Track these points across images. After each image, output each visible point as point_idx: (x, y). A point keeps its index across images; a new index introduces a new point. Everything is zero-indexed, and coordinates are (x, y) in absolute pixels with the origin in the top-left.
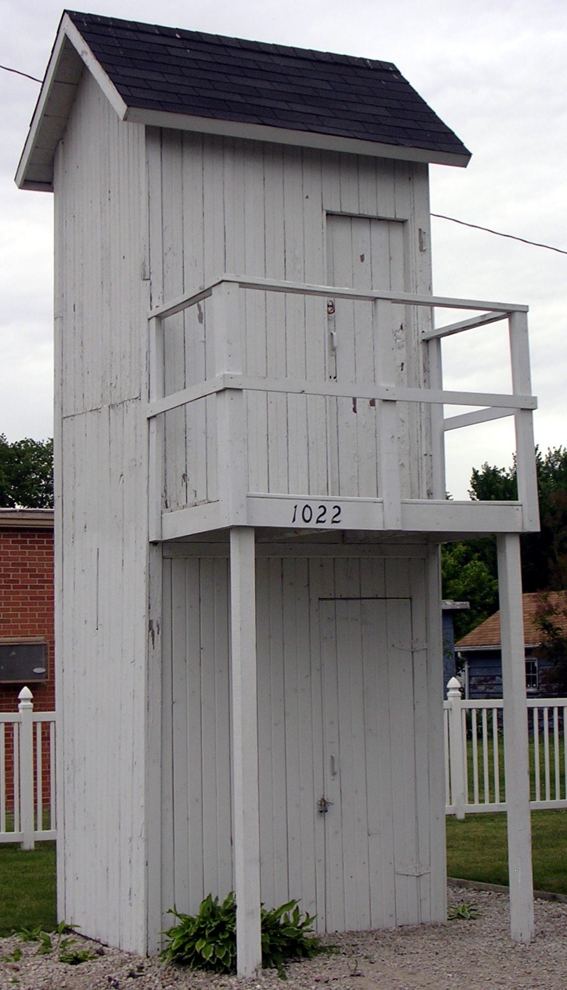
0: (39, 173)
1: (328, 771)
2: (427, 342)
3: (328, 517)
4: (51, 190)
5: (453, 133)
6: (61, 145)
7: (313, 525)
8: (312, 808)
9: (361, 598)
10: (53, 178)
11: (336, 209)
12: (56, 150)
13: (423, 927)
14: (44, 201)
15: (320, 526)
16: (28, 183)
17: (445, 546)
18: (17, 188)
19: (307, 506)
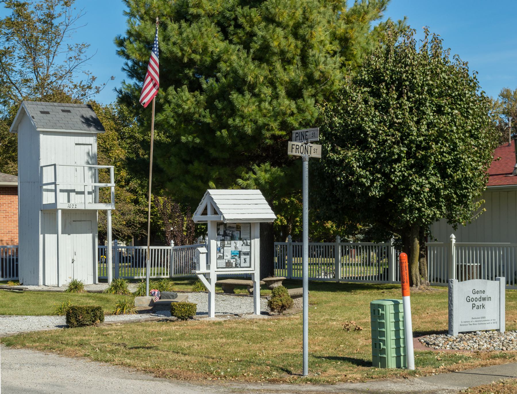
3: (74, 206)
6: (19, 126)
7: (71, 208)
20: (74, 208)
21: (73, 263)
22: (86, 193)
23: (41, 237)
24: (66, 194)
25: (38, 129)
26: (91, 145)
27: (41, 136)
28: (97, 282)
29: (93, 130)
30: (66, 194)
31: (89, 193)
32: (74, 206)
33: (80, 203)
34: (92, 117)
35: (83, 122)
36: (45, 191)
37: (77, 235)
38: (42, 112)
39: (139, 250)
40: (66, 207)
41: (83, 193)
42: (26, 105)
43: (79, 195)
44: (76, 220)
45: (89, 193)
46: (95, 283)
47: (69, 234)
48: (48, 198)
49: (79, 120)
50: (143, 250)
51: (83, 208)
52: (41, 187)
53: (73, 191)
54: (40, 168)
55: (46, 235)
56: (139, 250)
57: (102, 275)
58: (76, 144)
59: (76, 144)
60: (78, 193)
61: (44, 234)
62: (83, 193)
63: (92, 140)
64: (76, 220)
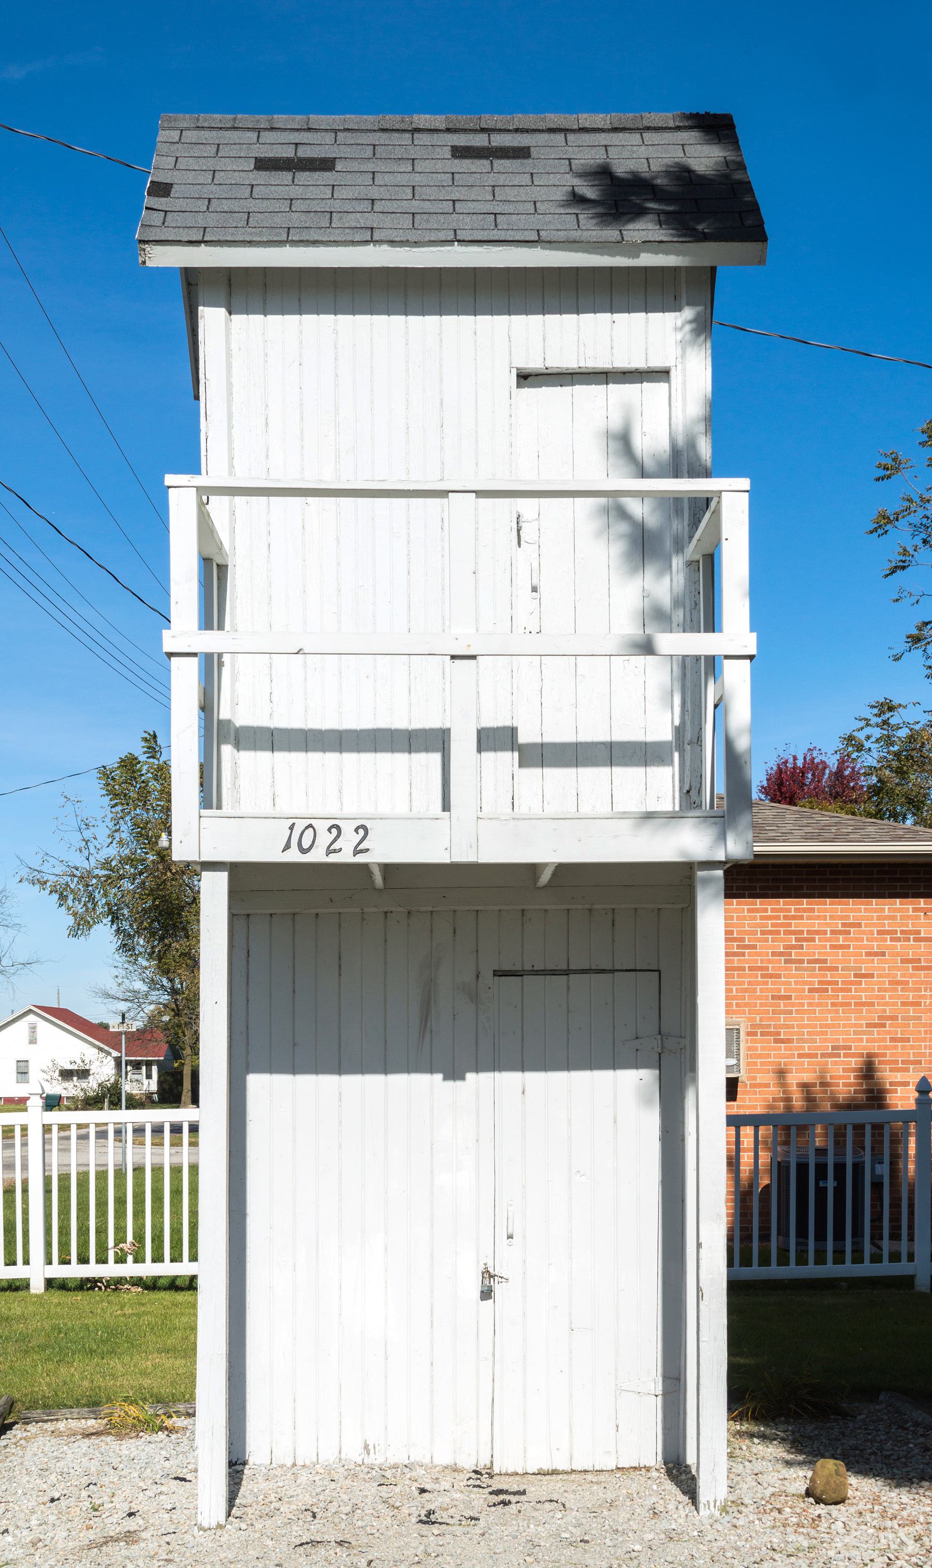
7: (317, 856)
9: (567, 972)
11: (534, 363)
15: (333, 858)
19: (310, 826)
20: (346, 856)
21: (487, 1294)
26: (662, 374)
29: (648, 245)
37: (534, 1078)
47: (454, 1074)
58: (525, 378)
59: (525, 378)
63: (658, 336)
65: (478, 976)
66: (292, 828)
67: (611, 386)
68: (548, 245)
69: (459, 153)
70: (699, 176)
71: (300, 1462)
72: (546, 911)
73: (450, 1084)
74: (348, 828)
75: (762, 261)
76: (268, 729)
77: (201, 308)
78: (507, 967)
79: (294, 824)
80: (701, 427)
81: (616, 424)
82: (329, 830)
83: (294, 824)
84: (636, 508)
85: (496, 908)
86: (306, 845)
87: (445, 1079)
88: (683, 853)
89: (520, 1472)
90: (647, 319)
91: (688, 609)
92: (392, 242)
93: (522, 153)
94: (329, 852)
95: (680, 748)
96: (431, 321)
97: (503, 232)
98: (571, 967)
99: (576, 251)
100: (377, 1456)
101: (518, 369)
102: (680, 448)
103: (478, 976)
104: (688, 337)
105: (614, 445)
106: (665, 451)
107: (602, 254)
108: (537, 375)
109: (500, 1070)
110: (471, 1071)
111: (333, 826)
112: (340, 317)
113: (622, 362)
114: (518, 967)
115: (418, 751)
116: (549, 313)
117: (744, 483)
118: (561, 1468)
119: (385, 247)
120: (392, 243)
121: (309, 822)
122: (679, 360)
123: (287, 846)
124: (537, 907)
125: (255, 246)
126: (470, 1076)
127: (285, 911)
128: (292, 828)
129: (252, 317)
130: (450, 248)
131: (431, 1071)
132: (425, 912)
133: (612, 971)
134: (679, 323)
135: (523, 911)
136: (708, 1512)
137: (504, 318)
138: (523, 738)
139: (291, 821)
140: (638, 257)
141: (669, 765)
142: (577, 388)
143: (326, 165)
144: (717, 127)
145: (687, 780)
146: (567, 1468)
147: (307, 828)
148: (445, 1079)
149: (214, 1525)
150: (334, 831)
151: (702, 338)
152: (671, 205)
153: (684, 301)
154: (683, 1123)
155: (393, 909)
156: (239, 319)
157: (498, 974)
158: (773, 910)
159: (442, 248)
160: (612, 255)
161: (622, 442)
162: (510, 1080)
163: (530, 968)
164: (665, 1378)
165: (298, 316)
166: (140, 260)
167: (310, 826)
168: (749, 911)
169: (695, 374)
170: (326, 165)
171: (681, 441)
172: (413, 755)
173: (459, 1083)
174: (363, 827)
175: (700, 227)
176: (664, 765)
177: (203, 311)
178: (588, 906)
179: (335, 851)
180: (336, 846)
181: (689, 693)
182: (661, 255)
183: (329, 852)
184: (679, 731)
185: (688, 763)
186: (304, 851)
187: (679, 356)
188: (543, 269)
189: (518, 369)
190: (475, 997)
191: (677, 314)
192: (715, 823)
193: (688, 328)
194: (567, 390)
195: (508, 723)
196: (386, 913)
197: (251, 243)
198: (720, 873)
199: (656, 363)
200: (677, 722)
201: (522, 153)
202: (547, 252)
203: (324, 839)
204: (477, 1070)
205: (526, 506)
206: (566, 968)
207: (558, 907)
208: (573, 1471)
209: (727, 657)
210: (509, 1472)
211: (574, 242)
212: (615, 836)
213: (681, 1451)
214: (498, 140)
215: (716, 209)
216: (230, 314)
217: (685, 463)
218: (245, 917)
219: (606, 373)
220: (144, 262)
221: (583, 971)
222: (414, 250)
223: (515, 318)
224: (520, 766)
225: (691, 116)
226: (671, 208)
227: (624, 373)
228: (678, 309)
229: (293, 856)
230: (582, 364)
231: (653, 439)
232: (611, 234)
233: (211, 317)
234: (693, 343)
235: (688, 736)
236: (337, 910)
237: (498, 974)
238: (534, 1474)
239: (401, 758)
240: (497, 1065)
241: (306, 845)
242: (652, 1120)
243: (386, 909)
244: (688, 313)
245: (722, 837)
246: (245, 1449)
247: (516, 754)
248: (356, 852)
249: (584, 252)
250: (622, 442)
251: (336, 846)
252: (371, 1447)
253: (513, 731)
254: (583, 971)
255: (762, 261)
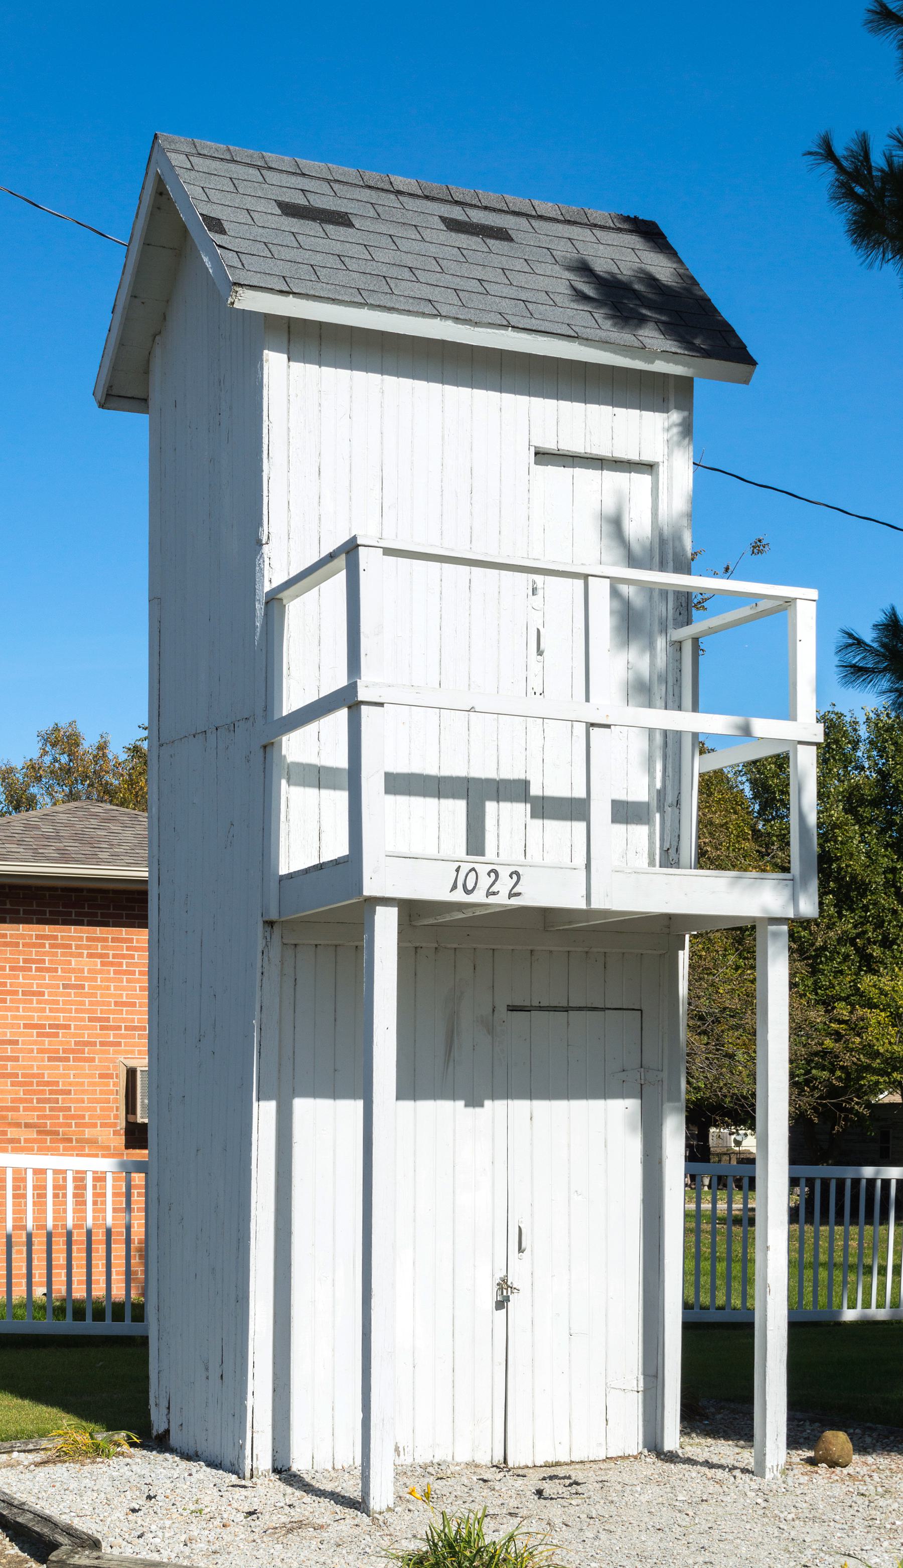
0: (122, 391)
1: (514, 1246)
2: (265, 747)
3: (504, 885)
4: (145, 410)
5: (732, 331)
6: (158, 351)
7: (479, 897)
8: (489, 1297)
9: (566, 1009)
10: (148, 392)
11: (550, 445)
12: (148, 361)
13: (628, 1457)
14: (135, 426)
15: (492, 900)
16: (113, 396)
17: (695, 937)
18: (96, 405)
19: (473, 869)
20: (502, 899)
21: (501, 1304)
22: (600, 811)
23: (264, 1114)
24: (459, 807)
25: (249, 301)
26: (649, 467)
27: (283, 377)
28: (672, 1439)
29: (656, 352)
30: (459, 807)
31: (625, 813)
32: (504, 885)
33: (547, 869)
34: (651, 280)
35: (581, 297)
36: (304, 783)
37: (541, 1106)
38: (289, 210)
39: (841, 1183)
40: (434, 887)
41: (574, 809)
42: (177, 160)
43: (552, 825)
44: (522, 995)
45: (625, 813)
46: (654, 1445)
47: (474, 1102)
48: (307, 829)
49: (561, 282)
50: (856, 1182)
51: (570, 898)
52: (269, 748)
53: (514, 790)
54: (261, 598)
55: (302, 1106)
56: (841, 1183)
57: (705, 1299)
58: (543, 456)
59: (543, 456)
60: (547, 808)
61: (258, 1100)
62: (574, 809)
63: (645, 431)
64: (522, 995)
65: (494, 1011)
66: (458, 870)
67: (605, 472)
68: (585, 342)
69: (453, 225)
70: (664, 285)
71: (338, 1466)
72: (551, 952)
73: (470, 1110)
74: (504, 873)
75: (746, 381)
76: (315, 766)
77: (266, 352)
78: (518, 1002)
79: (459, 867)
80: (685, 522)
81: (610, 507)
82: (489, 874)
83: (459, 867)
84: (624, 589)
85: (511, 947)
86: (470, 886)
87: (466, 1106)
88: (764, 910)
89: (530, 1465)
90: (641, 416)
91: (670, 683)
92: (457, 319)
93: (502, 235)
94: (489, 894)
95: (661, 809)
96: (464, 392)
97: (538, 322)
98: (571, 1005)
99: (605, 351)
100: (406, 1457)
101: (535, 447)
102: (665, 538)
103: (494, 1011)
104: (675, 438)
105: (606, 528)
106: (647, 538)
107: (625, 356)
108: (544, 454)
109: (512, 1098)
110: (488, 1099)
111: (492, 871)
112: (386, 377)
113: (621, 453)
114: (527, 1003)
115: (447, 797)
116: (562, 399)
117: (813, 594)
118: (562, 1460)
119: (450, 323)
120: (456, 320)
121: (472, 865)
122: (666, 457)
123: (454, 887)
124: (544, 948)
125: (337, 304)
126: (487, 1103)
127: (329, 942)
128: (458, 870)
129: (309, 366)
130: (503, 332)
131: (454, 1098)
132: (451, 949)
133: (604, 1009)
134: (666, 425)
135: (532, 951)
136: (772, 1475)
137: (525, 399)
138: (535, 791)
139: (458, 864)
140: (653, 363)
141: (645, 824)
142: (577, 470)
143: (342, 219)
144: (650, 233)
145: (667, 838)
146: (567, 1460)
147: (470, 871)
148: (466, 1106)
149: (384, 1508)
150: (493, 875)
151: (687, 440)
152: (660, 313)
153: (672, 403)
154: (661, 1148)
155: (424, 945)
156: (297, 366)
157: (512, 1009)
158: (89, 939)
159: (497, 331)
160: (633, 358)
161: (615, 525)
162: (521, 1107)
163: (537, 1004)
164: (645, 1374)
165: (349, 371)
166: (230, 300)
167: (473, 869)
168: (38, 937)
169: (679, 474)
170: (342, 219)
171: (666, 531)
172: (442, 800)
173: (478, 1110)
174: (516, 873)
175: (697, 342)
176: (642, 824)
177: (267, 355)
178: (586, 949)
179: (494, 894)
180: (494, 889)
181: (670, 761)
182: (671, 364)
183: (489, 894)
184: (661, 794)
185: (668, 824)
186: (468, 892)
187: (666, 453)
188: (572, 360)
189: (535, 447)
190: (491, 1030)
191: (665, 415)
192: (787, 885)
193: (675, 430)
194: (569, 471)
195: (522, 777)
196: (416, 948)
197: (333, 301)
198: (785, 928)
199: (646, 457)
200: (658, 785)
201: (502, 235)
202: (582, 348)
203: (485, 882)
204: (493, 1098)
205: (539, 579)
206: (566, 1005)
207: (561, 949)
208: (572, 1462)
209: (800, 743)
210: (521, 1465)
211: (607, 342)
212: (714, 892)
213: (659, 1441)
214: (478, 217)
215: (697, 324)
216: (289, 360)
217: (671, 551)
218: (293, 947)
219: (601, 460)
220: (233, 303)
221: (580, 1009)
222: (476, 329)
223: (534, 400)
224: (532, 817)
225: (627, 219)
226: (663, 318)
227: (616, 462)
228: (666, 410)
229: (459, 896)
230: (588, 451)
231: (639, 527)
232: (625, 337)
233: (274, 363)
234: (679, 444)
235: (670, 798)
236: (603, 950)
237: (512, 1009)
238: (541, 1467)
239: (431, 803)
240: (508, 1094)
241: (470, 887)
242: (635, 1146)
243: (418, 945)
244: (675, 416)
245: (794, 899)
246: (289, 1457)
247: (529, 806)
248: (511, 895)
249: (611, 352)
250: (615, 525)
251: (494, 889)
252: (401, 1449)
253: (526, 784)
254: (580, 1009)
255: (746, 381)
